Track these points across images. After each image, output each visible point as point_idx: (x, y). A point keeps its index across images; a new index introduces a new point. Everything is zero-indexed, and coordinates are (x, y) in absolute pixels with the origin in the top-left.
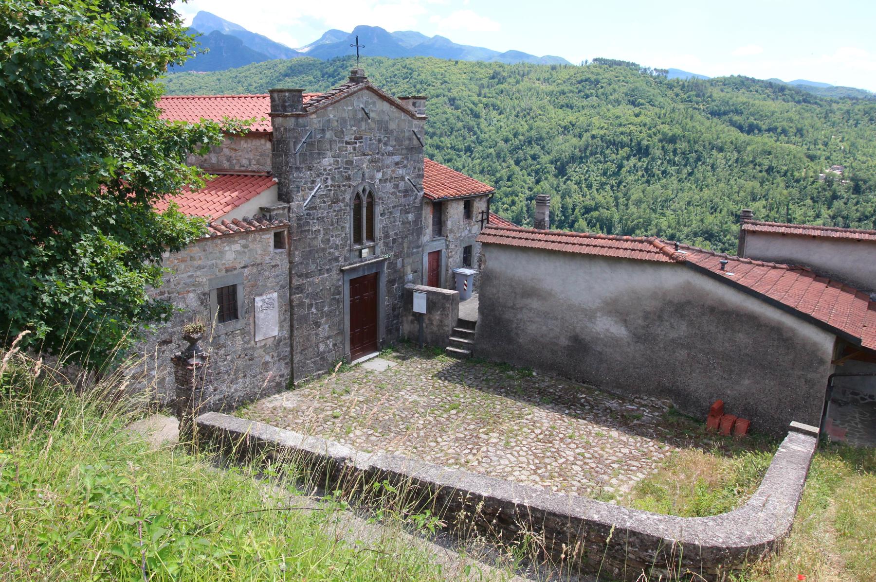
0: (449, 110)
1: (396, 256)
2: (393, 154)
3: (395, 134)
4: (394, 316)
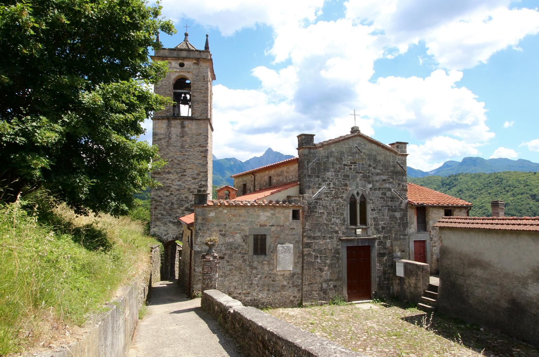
0: (532, 202)
1: (385, 238)
2: (381, 174)
3: (382, 163)
4: (385, 278)
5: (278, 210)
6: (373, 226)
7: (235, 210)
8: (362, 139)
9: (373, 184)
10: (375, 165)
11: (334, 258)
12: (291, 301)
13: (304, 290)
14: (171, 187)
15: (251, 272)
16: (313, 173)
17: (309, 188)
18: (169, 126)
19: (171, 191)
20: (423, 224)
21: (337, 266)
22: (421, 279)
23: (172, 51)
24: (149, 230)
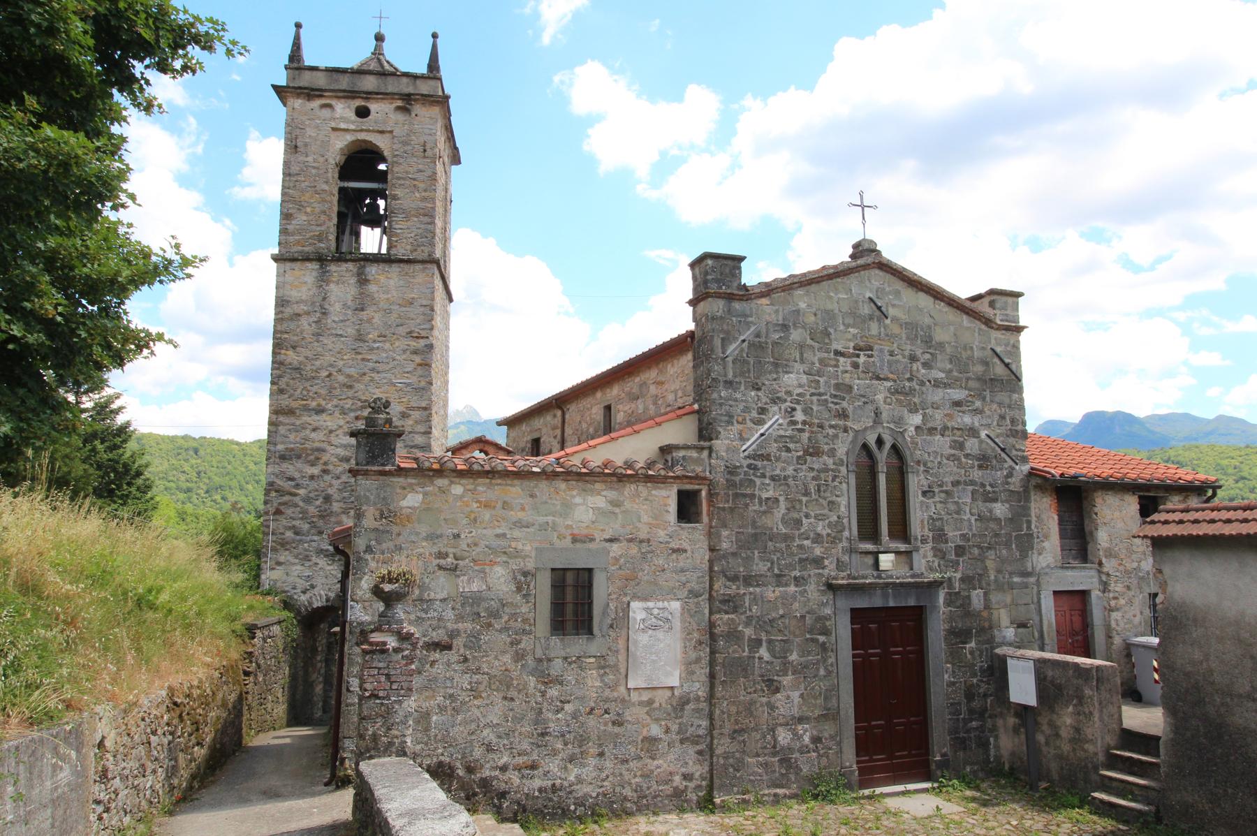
2: (946, 386)
3: (949, 350)
4: (971, 711)
5: (630, 489)
7: (490, 486)
8: (888, 276)
9: (924, 415)
10: (927, 356)
11: (812, 647)
12: (676, 788)
13: (718, 752)
14: (324, 451)
15: (543, 694)
16: (742, 374)
17: (730, 423)
18: (323, 278)
19: (325, 464)
20: (1079, 541)
21: (822, 672)
22: (1096, 714)
23: (335, 75)
24: (257, 577)
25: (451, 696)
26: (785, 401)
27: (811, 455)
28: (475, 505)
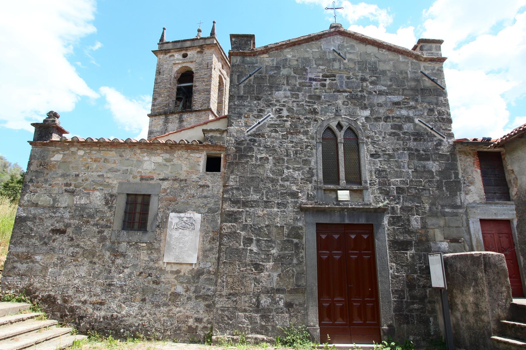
4: (413, 297)
5: (178, 153)
6: (377, 187)
16: (249, 92)
18: (166, 122)
21: (295, 261)
25: (61, 259)
26: (276, 105)
27: (291, 134)
28: (89, 160)
